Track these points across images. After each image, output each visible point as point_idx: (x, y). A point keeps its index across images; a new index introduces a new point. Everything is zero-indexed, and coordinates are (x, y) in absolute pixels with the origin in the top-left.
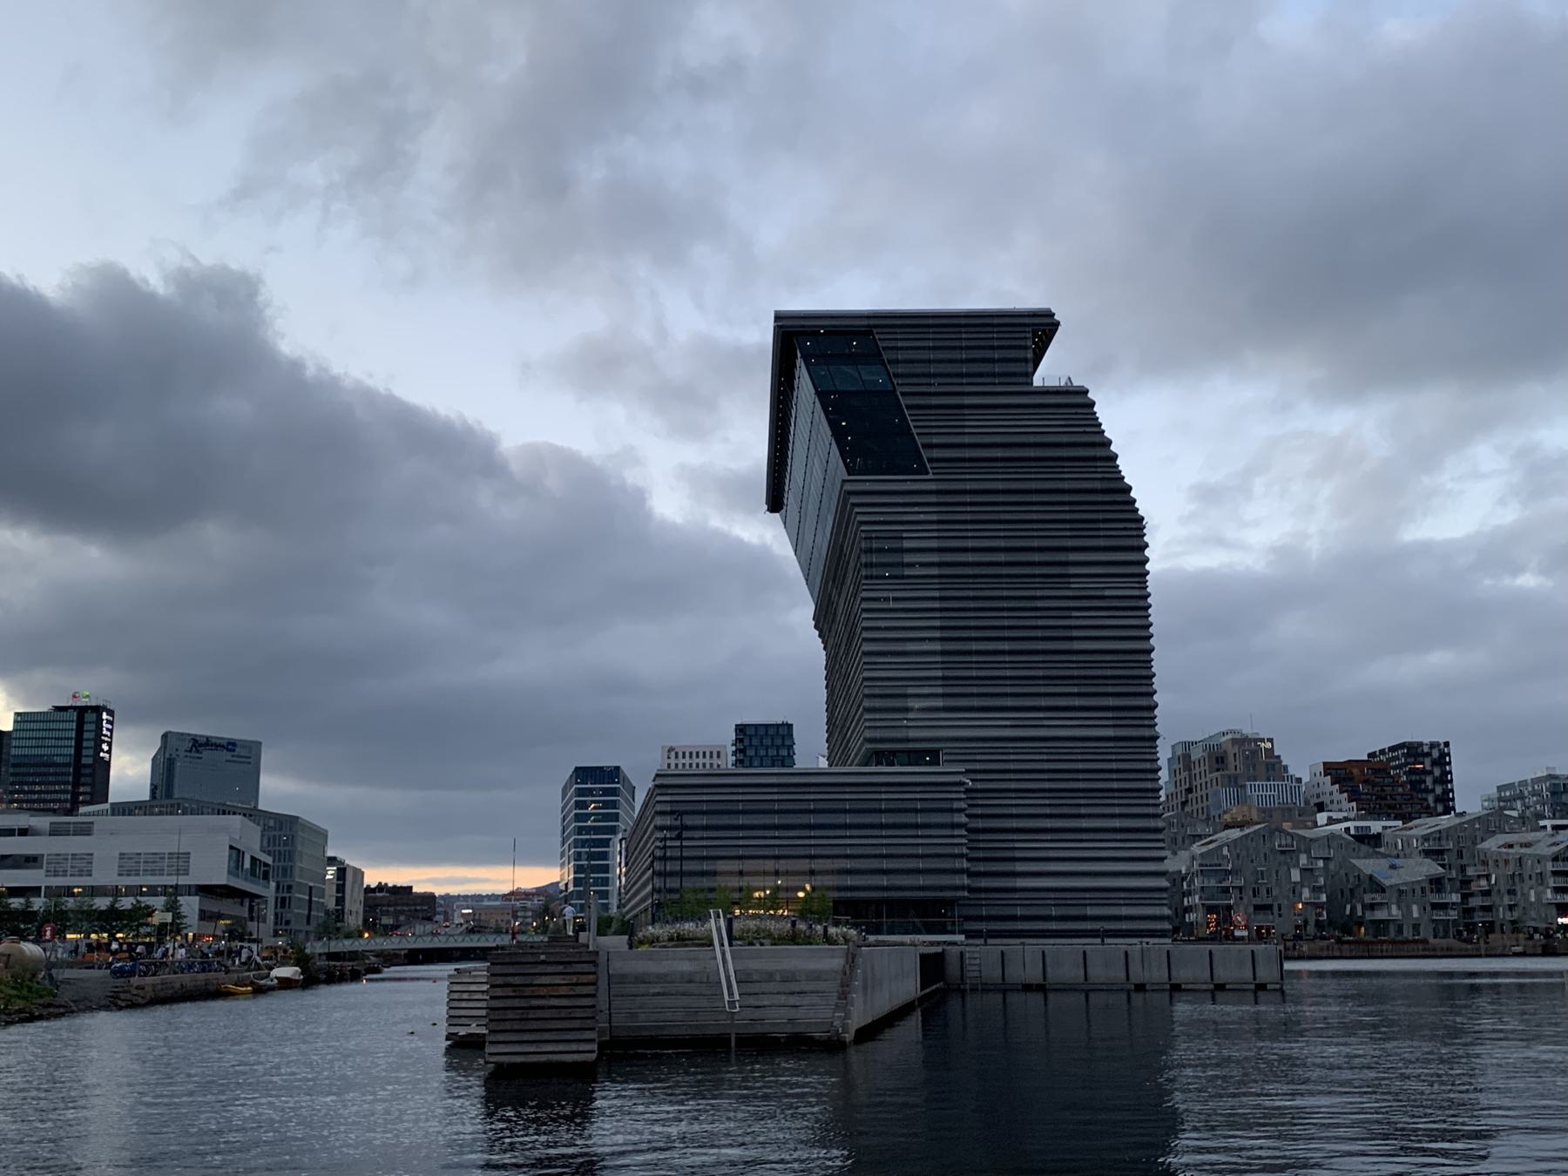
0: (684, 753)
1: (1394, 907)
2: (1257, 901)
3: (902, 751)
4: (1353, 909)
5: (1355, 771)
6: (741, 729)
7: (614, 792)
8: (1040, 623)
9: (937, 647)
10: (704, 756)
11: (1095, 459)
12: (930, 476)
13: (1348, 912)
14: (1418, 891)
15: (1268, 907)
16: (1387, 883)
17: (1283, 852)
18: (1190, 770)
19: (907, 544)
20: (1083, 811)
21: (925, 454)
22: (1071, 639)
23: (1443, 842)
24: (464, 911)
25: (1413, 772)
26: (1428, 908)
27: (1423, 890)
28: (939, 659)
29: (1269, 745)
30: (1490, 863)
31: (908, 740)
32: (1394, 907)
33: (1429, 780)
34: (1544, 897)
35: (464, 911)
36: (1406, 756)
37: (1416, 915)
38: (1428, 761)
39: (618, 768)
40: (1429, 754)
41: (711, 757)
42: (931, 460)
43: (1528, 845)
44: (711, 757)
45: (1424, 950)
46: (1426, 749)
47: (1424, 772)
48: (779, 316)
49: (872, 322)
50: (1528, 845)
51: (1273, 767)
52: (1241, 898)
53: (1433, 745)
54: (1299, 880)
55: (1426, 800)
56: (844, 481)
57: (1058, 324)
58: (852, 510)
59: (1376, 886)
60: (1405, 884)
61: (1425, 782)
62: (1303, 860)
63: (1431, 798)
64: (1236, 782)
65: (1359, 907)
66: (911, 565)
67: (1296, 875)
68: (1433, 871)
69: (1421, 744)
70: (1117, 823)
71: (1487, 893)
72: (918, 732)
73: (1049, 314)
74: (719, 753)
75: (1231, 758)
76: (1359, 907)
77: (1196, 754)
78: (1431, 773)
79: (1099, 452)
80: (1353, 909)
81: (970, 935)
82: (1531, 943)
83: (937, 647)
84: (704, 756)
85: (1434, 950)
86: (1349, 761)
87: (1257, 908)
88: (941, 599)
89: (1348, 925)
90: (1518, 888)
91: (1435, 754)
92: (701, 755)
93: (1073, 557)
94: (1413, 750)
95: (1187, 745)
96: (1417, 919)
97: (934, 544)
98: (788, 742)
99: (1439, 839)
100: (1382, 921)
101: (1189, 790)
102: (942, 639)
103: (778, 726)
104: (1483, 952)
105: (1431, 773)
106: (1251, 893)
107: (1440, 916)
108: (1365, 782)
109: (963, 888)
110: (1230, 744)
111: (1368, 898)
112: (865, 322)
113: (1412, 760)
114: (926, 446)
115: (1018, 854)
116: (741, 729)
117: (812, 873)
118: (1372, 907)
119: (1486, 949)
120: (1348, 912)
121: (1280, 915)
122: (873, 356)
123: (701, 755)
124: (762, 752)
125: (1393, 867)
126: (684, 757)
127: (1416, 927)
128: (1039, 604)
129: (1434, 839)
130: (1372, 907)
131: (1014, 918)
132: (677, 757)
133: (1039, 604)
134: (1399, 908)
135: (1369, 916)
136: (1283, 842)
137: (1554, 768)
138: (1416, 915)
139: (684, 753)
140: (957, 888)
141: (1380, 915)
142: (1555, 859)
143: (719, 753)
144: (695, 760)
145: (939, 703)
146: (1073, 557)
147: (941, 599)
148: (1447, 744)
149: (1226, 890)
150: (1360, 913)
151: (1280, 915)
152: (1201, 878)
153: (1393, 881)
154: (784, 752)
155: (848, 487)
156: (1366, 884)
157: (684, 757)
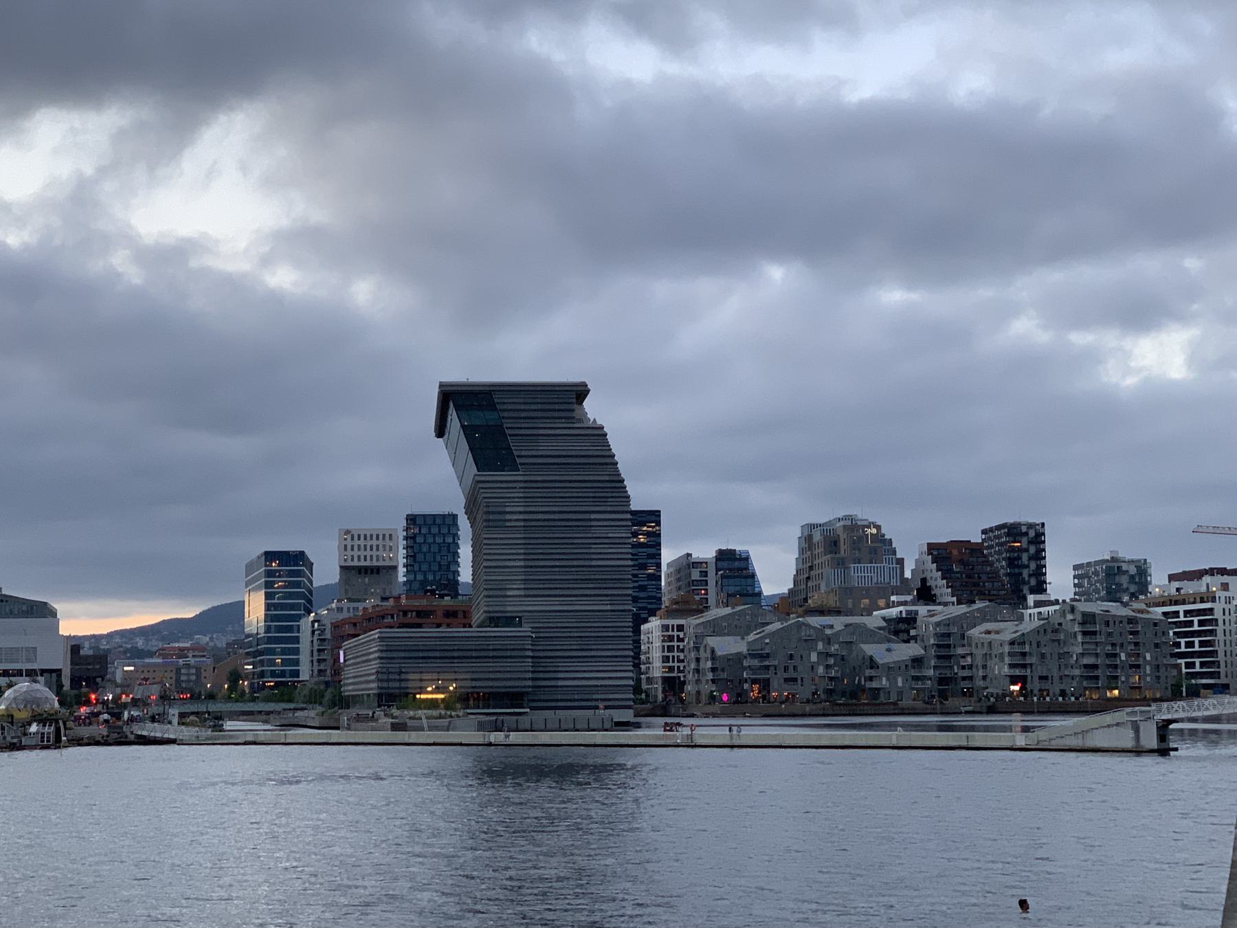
0: (359, 536)
1: (884, 679)
2: (786, 675)
3: (503, 617)
4: (860, 680)
5: (955, 552)
6: (412, 519)
7: (298, 573)
8: (572, 551)
9: (522, 563)
10: (378, 538)
11: (606, 464)
12: (521, 473)
13: (856, 682)
14: (903, 667)
15: (795, 680)
16: (880, 662)
17: (806, 640)
18: (812, 551)
19: (508, 509)
20: (593, 647)
21: (518, 461)
22: (591, 559)
23: (951, 627)
24: (126, 668)
25: (1013, 549)
26: (910, 679)
27: (906, 666)
28: (523, 570)
29: (874, 531)
30: (974, 645)
31: (506, 612)
32: (884, 679)
33: (1025, 557)
34: (1002, 671)
35: (126, 668)
36: (1008, 534)
37: (900, 684)
38: (1025, 540)
39: (302, 553)
40: (1026, 534)
41: (384, 539)
42: (521, 464)
43: (997, 632)
44: (384, 539)
45: (894, 709)
46: (1024, 529)
47: (1020, 550)
48: (441, 385)
49: (491, 389)
50: (997, 632)
51: (880, 547)
52: (776, 673)
53: (1030, 526)
54: (816, 660)
55: (1021, 574)
56: (476, 475)
57: (589, 391)
58: (478, 491)
59: (873, 664)
60: (894, 662)
61: (1020, 558)
62: (820, 646)
63: (1025, 573)
64: (843, 564)
65: (863, 680)
66: (510, 520)
67: (814, 657)
68: (916, 653)
69: (1020, 524)
70: (609, 653)
71: (970, 667)
72: (511, 609)
73: (584, 385)
74: (390, 535)
75: (842, 543)
76: (863, 680)
77: (817, 537)
78: (1027, 550)
79: (608, 460)
80: (860, 680)
81: (532, 708)
82: (979, 704)
83: (522, 563)
84: (378, 538)
85: (903, 709)
86: (951, 541)
87: (786, 680)
88: (525, 538)
89: (855, 693)
90: (988, 664)
91: (1032, 534)
92: (374, 537)
93: (593, 516)
94: (1013, 530)
95: (813, 526)
96: (900, 688)
97: (521, 509)
98: (453, 531)
99: (949, 625)
100: (876, 689)
101: (811, 568)
102: (524, 560)
103: (444, 517)
104: (1036, 710)
105: (1027, 550)
106: (783, 669)
107: (920, 685)
108: (961, 562)
109: (529, 687)
110: (842, 529)
111: (868, 672)
112: (488, 389)
113: (1011, 539)
114: (518, 456)
115: (560, 669)
116: (412, 519)
117: (456, 680)
118: (871, 679)
119: (942, 709)
120: (856, 682)
121: (802, 685)
122: (492, 406)
123: (374, 537)
124: (430, 540)
125: (889, 650)
126: (359, 539)
127: (900, 693)
128: (576, 541)
129: (945, 625)
130: (871, 679)
131: (557, 700)
132: (352, 539)
133: (576, 541)
134: (888, 679)
135: (870, 685)
136: (808, 633)
137: (1117, 552)
138: (900, 684)
139: (359, 536)
140: (524, 687)
141: (874, 685)
142: (1012, 643)
143: (390, 535)
144: (374, 542)
145: (522, 593)
146: (593, 516)
147: (525, 538)
148: (1043, 524)
149: (767, 668)
150: (863, 683)
151: (802, 685)
152: (748, 659)
153: (886, 661)
154: (450, 540)
155: (478, 478)
156: (867, 663)
157: (359, 539)
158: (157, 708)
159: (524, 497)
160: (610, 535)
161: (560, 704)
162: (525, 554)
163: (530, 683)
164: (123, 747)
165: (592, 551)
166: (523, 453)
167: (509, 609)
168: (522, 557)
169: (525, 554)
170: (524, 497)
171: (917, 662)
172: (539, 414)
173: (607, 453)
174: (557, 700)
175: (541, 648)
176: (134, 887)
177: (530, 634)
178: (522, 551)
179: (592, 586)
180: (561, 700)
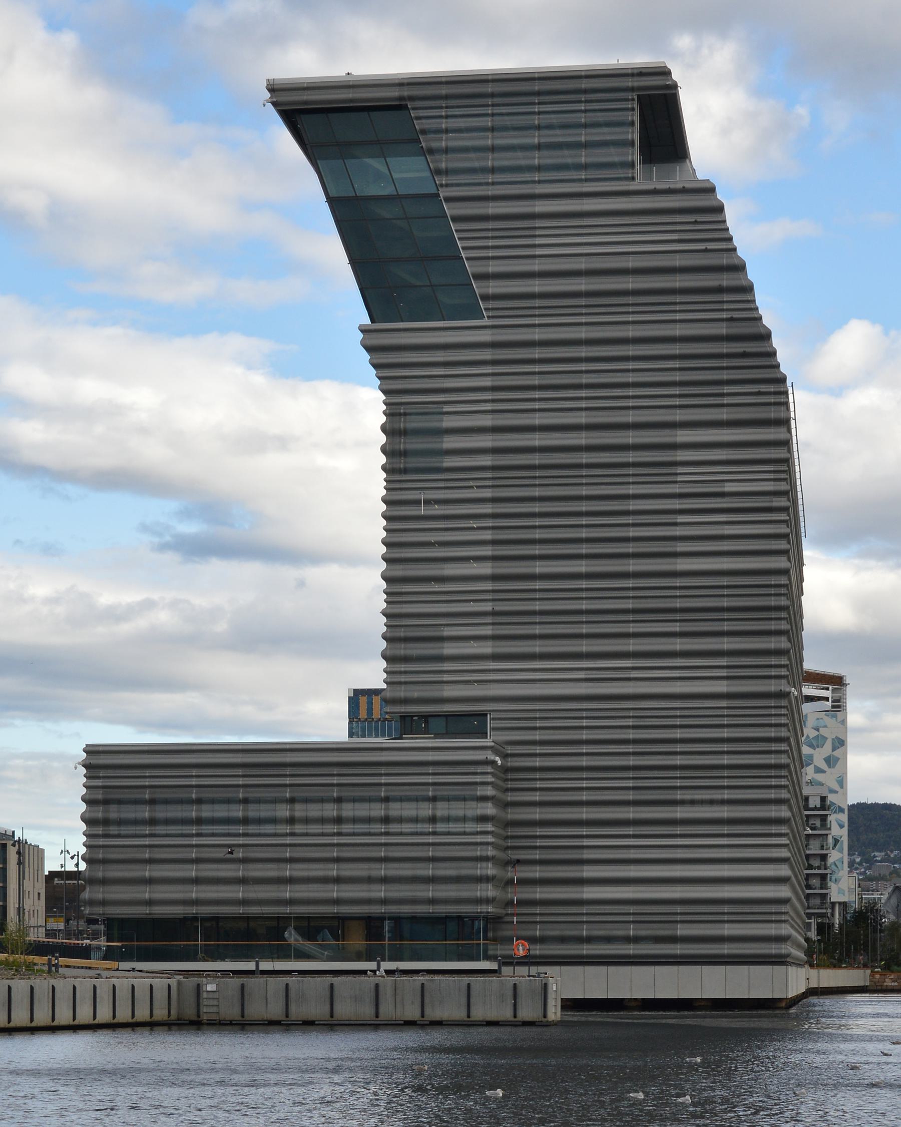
9: (486, 569)
12: (486, 322)
19: (448, 422)
20: (679, 795)
48: (824, 759)
49: (406, 92)
79: (725, 280)
83: (486, 569)
88: (494, 500)
93: (683, 436)
97: (487, 421)
114: (479, 277)
128: (632, 505)
158: (30, 935)
159: (494, 389)
160: (729, 488)
161: (586, 950)
162: (494, 542)
163: (490, 891)
164: (674, 996)
165: (678, 531)
166: (493, 267)
167: (449, 692)
168: (487, 551)
169: (494, 542)
170: (494, 389)
171: (563, 1081)
172: (677, 402)
173: (725, 260)
174: (580, 940)
175: (537, 797)
176: (697, 1070)
177: (491, 757)
178: (488, 536)
179: (677, 628)
180: (589, 940)
